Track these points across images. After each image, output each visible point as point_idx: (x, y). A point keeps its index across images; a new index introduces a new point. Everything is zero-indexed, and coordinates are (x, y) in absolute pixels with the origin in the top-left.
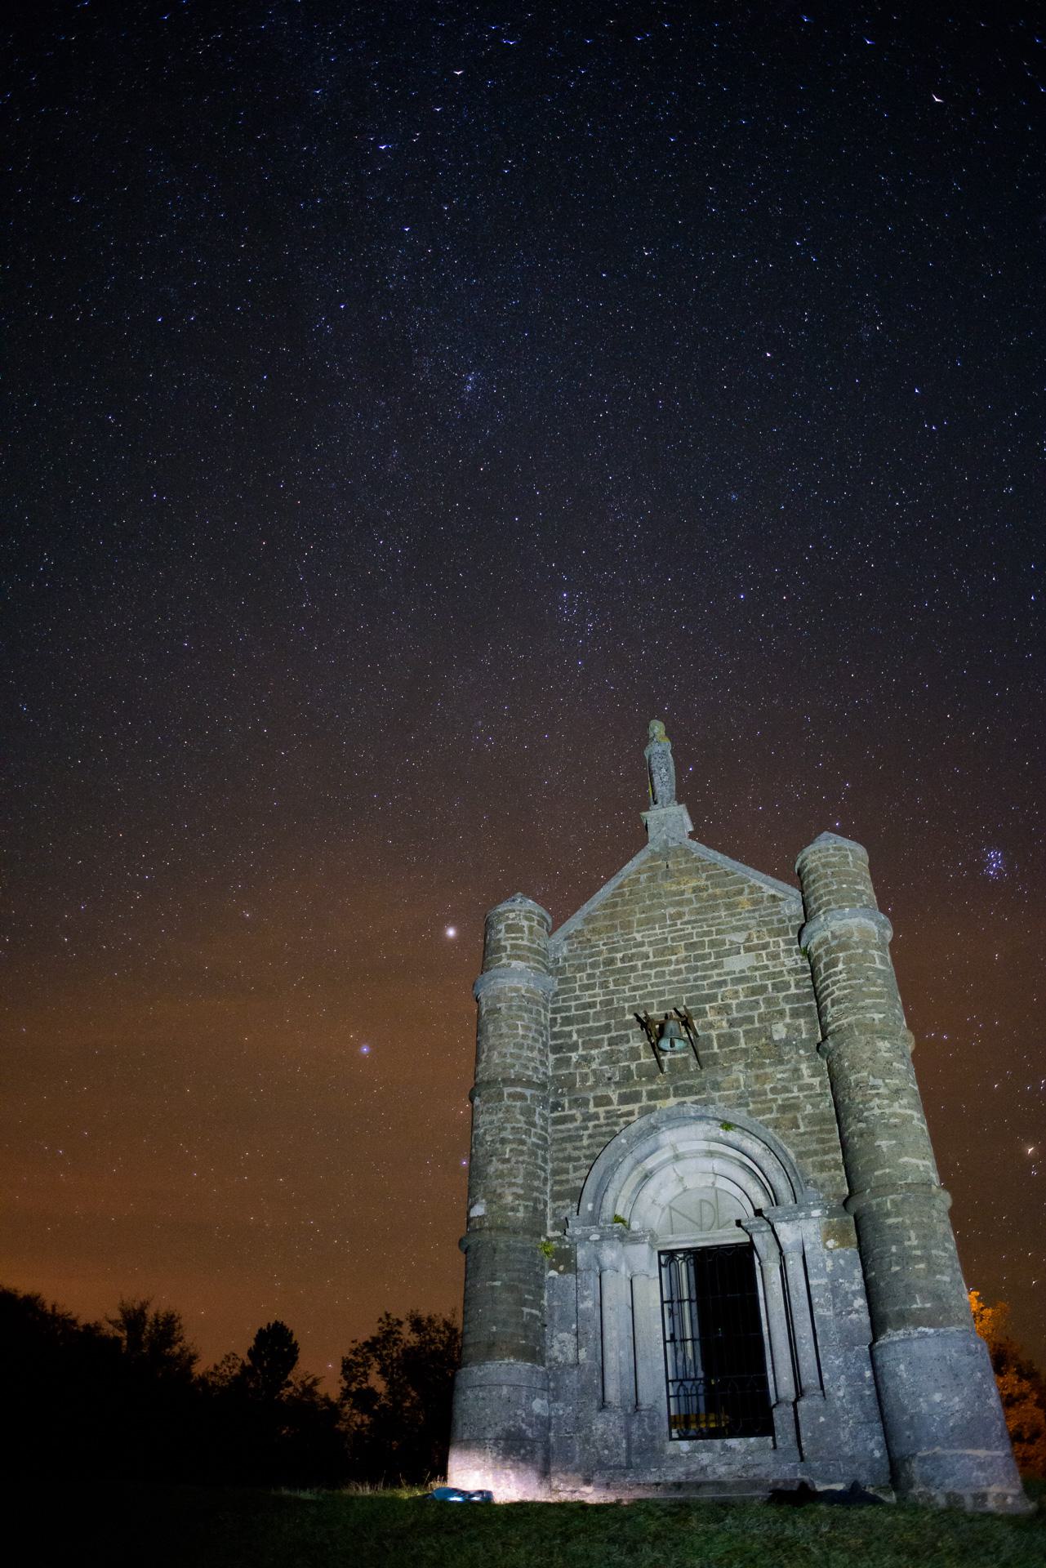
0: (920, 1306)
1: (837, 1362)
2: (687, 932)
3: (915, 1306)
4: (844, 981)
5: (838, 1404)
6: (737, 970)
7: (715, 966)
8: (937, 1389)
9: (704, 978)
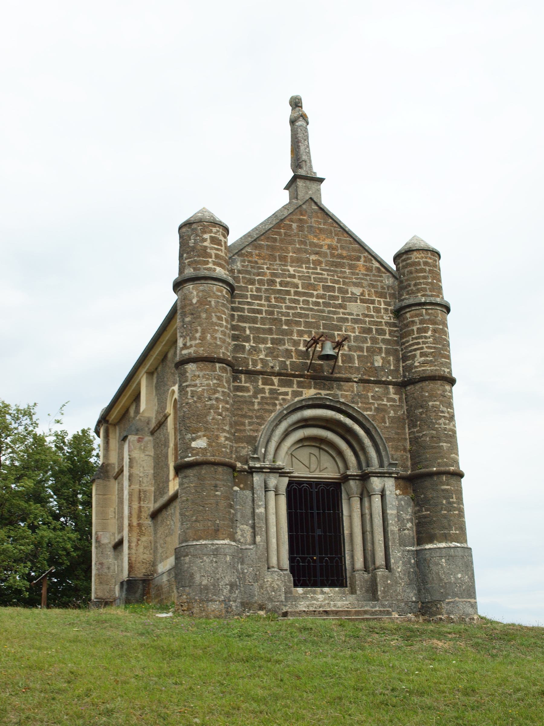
0: (454, 532)
1: (398, 554)
2: (323, 276)
3: (452, 532)
4: (431, 343)
5: (398, 575)
6: (355, 313)
7: (341, 306)
8: (459, 572)
9: (335, 313)
